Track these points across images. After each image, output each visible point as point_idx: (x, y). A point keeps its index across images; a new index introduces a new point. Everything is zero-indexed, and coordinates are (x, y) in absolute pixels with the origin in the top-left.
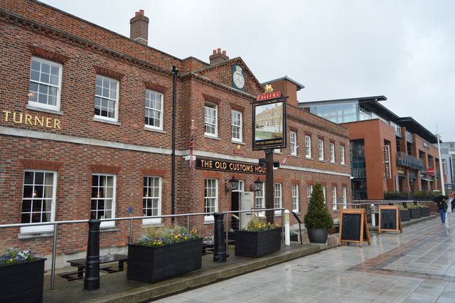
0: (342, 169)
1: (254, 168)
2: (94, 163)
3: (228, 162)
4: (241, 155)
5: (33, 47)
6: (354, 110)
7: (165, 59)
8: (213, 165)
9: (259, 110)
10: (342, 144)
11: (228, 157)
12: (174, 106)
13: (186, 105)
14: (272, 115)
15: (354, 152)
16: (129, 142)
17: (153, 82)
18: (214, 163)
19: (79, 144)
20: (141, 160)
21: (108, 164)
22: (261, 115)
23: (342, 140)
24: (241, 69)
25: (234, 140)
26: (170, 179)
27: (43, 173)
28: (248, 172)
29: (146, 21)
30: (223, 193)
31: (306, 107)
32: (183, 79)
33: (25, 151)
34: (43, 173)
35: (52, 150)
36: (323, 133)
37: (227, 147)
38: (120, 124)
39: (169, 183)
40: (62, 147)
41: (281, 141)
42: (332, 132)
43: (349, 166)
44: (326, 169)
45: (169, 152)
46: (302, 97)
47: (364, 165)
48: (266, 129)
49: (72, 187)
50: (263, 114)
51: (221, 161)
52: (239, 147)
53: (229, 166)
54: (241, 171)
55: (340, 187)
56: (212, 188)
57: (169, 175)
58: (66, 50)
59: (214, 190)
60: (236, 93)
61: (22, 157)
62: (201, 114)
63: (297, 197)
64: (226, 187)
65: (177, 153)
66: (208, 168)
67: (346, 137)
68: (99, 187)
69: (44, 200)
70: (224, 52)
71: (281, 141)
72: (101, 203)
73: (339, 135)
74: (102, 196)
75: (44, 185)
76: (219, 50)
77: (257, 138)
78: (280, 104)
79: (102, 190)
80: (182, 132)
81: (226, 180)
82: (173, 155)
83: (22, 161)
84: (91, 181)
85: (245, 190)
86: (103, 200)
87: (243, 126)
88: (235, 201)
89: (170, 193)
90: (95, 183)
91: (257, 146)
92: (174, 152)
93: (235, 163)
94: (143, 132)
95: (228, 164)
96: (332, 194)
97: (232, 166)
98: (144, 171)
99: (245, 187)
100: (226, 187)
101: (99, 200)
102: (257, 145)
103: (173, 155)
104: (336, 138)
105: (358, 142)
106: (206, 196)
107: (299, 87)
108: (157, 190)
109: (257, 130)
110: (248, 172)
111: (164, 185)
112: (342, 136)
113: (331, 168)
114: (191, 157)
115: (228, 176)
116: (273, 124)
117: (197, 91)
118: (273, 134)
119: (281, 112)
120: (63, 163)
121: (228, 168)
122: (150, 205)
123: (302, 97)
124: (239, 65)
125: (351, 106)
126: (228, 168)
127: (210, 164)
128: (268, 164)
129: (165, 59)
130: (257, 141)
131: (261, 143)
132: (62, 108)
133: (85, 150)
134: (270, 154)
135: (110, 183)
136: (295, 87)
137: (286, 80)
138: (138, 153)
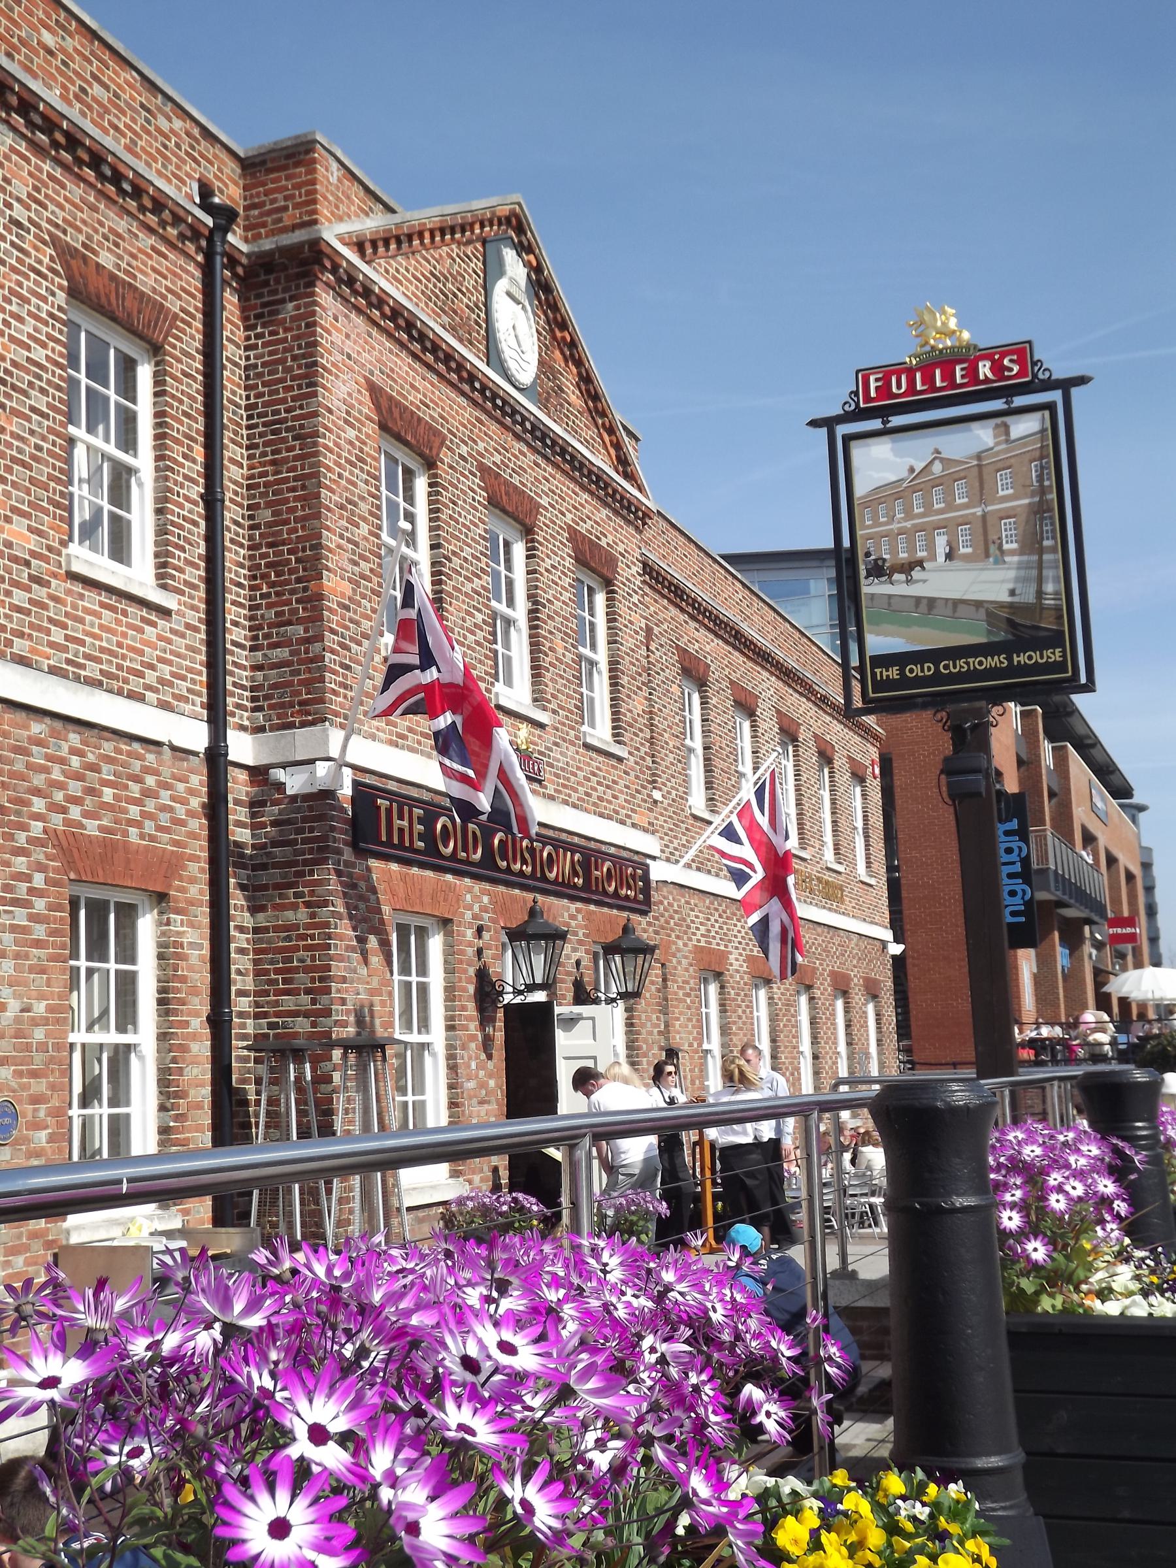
7: (163, 123)
8: (429, 836)
14: (982, 490)
17: (106, 259)
18: (429, 820)
20: (56, 775)
26: (203, 914)
27: (107, 902)
34: (107, 902)
39: (195, 938)
48: (942, 581)
50: (919, 483)
56: (414, 979)
62: (364, 508)
65: (242, 747)
77: (879, 642)
81: (480, 931)
82: (216, 757)
87: (533, 615)
89: (201, 1005)
94: (58, 586)
98: (69, 848)
109: (870, 588)
111: (167, 955)
116: (988, 548)
118: (990, 611)
129: (163, 123)
130: (883, 661)
138: (38, 728)
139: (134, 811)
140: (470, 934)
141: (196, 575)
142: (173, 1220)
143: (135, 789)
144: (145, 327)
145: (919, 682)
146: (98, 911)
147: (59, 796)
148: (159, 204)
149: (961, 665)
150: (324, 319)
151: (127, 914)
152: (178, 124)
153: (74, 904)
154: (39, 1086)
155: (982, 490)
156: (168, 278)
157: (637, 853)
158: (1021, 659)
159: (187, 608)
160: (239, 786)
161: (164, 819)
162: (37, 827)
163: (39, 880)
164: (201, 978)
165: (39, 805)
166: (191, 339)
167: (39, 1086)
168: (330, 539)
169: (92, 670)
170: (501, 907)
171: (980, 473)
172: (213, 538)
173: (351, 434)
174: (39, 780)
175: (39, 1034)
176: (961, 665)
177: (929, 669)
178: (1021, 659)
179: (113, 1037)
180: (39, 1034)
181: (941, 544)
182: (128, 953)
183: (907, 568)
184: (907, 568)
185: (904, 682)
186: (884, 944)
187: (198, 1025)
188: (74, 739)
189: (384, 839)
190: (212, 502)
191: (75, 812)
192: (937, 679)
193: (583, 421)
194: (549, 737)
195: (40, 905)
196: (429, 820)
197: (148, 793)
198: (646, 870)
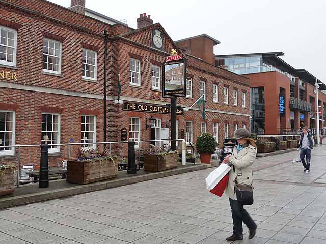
2: (43, 105)
6: (259, 63)
8: (137, 108)
12: (105, 62)
14: (177, 72)
18: (137, 106)
19: (31, 91)
20: (80, 103)
21: (54, 106)
26: (103, 118)
34: (89, 117)
35: (11, 96)
36: (227, 83)
39: (102, 121)
45: (103, 97)
46: (218, 51)
48: (172, 82)
58: (16, 17)
60: (155, 52)
70: (149, 16)
73: (241, 84)
76: (145, 14)
77: (166, 89)
78: (182, 64)
82: (105, 99)
84: (41, 119)
88: (153, 134)
92: (105, 97)
93: (154, 105)
95: (148, 107)
97: (151, 108)
101: (6, 132)
103: (105, 99)
104: (238, 86)
107: (216, 43)
111: (98, 123)
113: (234, 109)
116: (177, 79)
117: (124, 50)
118: (178, 86)
123: (218, 51)
130: (166, 91)
133: (36, 95)
134: (174, 101)
137: (205, 37)
138: (77, 98)
139: (92, 106)
142: (15, 177)
146: (134, 119)
147: (80, 105)
149: (174, 92)
150: (248, 211)
151: (137, 119)
153: (130, 119)
155: (177, 72)
157: (275, 154)
161: (97, 107)
162: (77, 109)
165: (77, 107)
166: (103, 50)
176: (174, 92)
187: (102, 130)
188: (83, 99)
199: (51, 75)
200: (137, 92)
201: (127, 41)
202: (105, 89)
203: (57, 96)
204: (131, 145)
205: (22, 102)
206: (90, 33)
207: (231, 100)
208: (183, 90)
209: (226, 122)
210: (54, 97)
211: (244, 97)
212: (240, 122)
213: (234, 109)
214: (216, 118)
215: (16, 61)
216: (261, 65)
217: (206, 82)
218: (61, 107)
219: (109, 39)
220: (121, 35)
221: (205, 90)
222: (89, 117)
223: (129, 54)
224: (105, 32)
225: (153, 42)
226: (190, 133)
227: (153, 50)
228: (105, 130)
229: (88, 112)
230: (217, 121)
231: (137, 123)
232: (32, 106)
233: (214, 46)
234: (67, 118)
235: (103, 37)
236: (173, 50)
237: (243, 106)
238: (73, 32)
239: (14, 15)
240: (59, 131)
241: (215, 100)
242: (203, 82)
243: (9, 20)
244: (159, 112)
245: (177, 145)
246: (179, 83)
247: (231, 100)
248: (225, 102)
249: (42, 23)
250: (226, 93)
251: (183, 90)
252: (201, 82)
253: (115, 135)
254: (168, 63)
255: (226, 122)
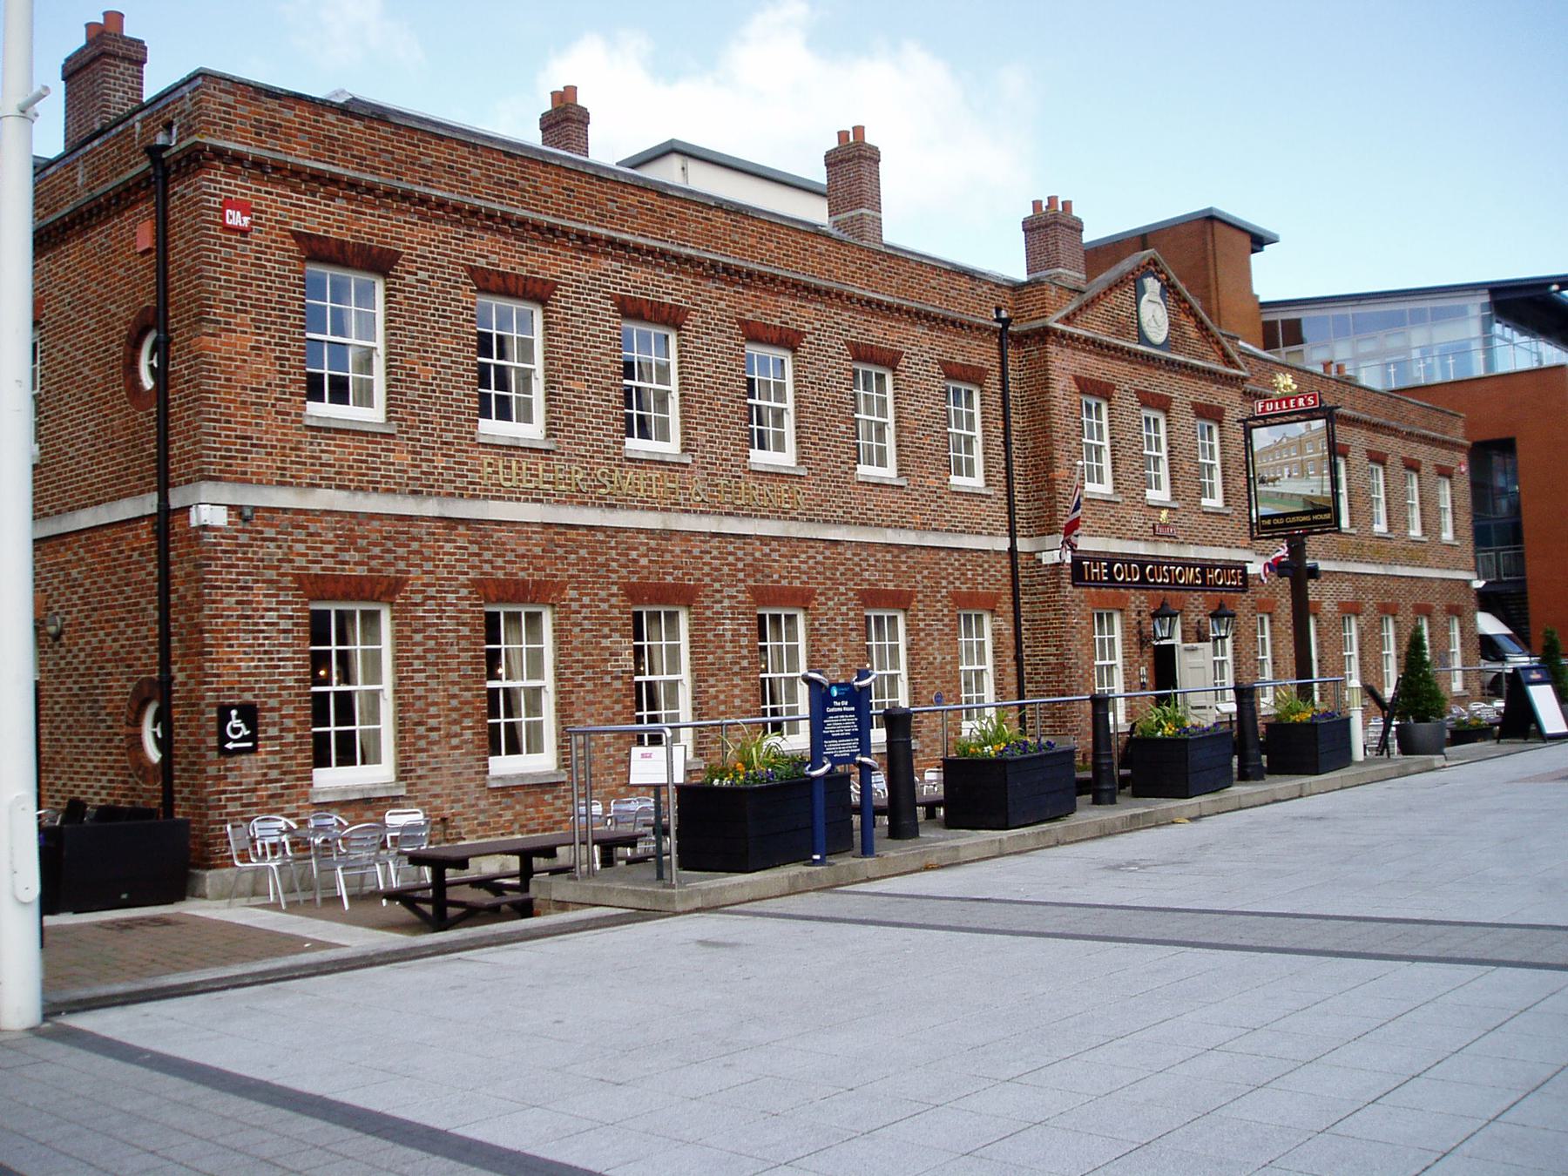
0: (1446, 556)
1: (1203, 573)
2: (865, 586)
3: (1142, 562)
4: (1172, 539)
5: (747, 322)
6: (1474, 328)
8: (1110, 574)
9: (1263, 437)
10: (1445, 472)
11: (1141, 549)
12: (1006, 418)
13: (1040, 412)
14: (1301, 451)
15: (1481, 492)
16: (924, 527)
17: (959, 359)
18: (1110, 567)
19: (836, 542)
21: (891, 586)
22: (1269, 451)
23: (1444, 457)
24: (1157, 285)
25: (1152, 495)
26: (1010, 616)
28: (1190, 587)
29: (873, 156)
30: (1135, 648)
31: (1283, 328)
32: (1021, 340)
33: (754, 569)
34: (498, 614)
36: (1384, 443)
37: (1136, 519)
38: (902, 482)
39: (1007, 628)
40: (811, 552)
41: (1328, 516)
42: (1409, 436)
43: (1469, 547)
44: (1395, 561)
45: (1003, 544)
46: (1271, 278)
47: (1513, 533)
48: (1287, 486)
49: (833, 646)
51: (1127, 559)
52: (1164, 513)
53: (1144, 572)
54: (1174, 585)
55: (1440, 618)
57: (1006, 606)
59: (894, 650)
60: (1148, 360)
61: (751, 582)
63: (1268, 656)
64: (1140, 632)
65: (1023, 545)
66: (1097, 583)
67: (1453, 446)
68: (334, 648)
69: (649, 683)
70: (1067, 205)
71: (1328, 516)
72: (345, 700)
73: (1433, 442)
74: (346, 677)
75: (503, 646)
76: (1053, 200)
78: (1319, 424)
79: (344, 658)
80: (1034, 482)
81: (1139, 613)
82: (1013, 551)
83: (753, 590)
84: (303, 632)
85: (1184, 640)
86: (349, 694)
88: (1164, 667)
89: (1010, 653)
90: (320, 636)
91: (1265, 528)
92: (1013, 542)
93: (1158, 562)
95: (1143, 566)
96: (1342, 644)
99: (1183, 631)
100: (1140, 632)
101: (336, 693)
102: (1265, 527)
103: (1013, 551)
104: (1421, 452)
105: (1489, 454)
106: (493, 676)
107: (1258, 241)
108: (373, 660)
110: (1190, 587)
111: (997, 634)
112: (1443, 444)
113: (1415, 552)
114: (1053, 554)
115: (1138, 600)
116: (1303, 474)
117: (1064, 365)
118: (1308, 500)
119: (1323, 446)
120: (813, 591)
121: (1143, 579)
122: (346, 715)
123: (1271, 278)
124: (1152, 274)
125: (1461, 313)
126: (1143, 579)
127: (1099, 570)
128: (1296, 572)
130: (1264, 517)
131: (1276, 521)
132: (802, 459)
134: (1297, 550)
135: (372, 633)
136: (1246, 241)
137: (1210, 220)
138: (942, 554)
140: (1134, 615)
141: (1000, 477)
143: (980, 571)
144: (975, 376)
145: (1278, 526)
148: (979, 327)
149: (1294, 520)
152: (985, 288)
154: (950, 686)
155: (1301, 451)
156: (982, 354)
158: (1316, 517)
159: (998, 492)
160: (1022, 561)
163: (946, 611)
164: (1011, 642)
165: (944, 583)
167: (950, 686)
168: (1057, 454)
169: (961, 527)
170: (1151, 601)
171: (1300, 444)
172: (1008, 460)
173: (1066, 403)
174: (944, 574)
175: (949, 667)
176: (1294, 520)
177: (1281, 521)
178: (1316, 517)
179: (976, 667)
180: (949, 667)
181: (1286, 470)
182: (980, 634)
183: (1273, 480)
184: (1273, 480)
185: (1272, 526)
186: (1467, 583)
187: (1010, 661)
188: (956, 555)
189: (855, 799)
190: (1007, 444)
191: (957, 583)
192: (1285, 525)
193: (1201, 347)
194: (1179, 514)
195: (946, 620)
196: (1110, 567)
197: (985, 571)
198: (1245, 569)
199: (877, 485)
200: (1107, 515)
201: (1071, 336)
202: (1011, 512)
203: (896, 552)
204: (1101, 704)
205: (820, 578)
206: (970, 327)
207: (1396, 517)
208: (1327, 510)
209: (1385, 612)
210: (889, 557)
211: (1445, 492)
212: (1438, 606)
213: (1415, 552)
214: (1348, 593)
215: (794, 451)
216: (1488, 341)
217: (1166, 412)
218: (905, 587)
219: (1011, 335)
220: (1054, 322)
221: (1106, 443)
222: (498, 614)
223: (1077, 379)
224: (998, 310)
225: (1139, 327)
226: (979, 674)
227: (1142, 354)
228: (1018, 659)
229: (515, 591)
230: (1351, 609)
231: (792, 635)
232: (842, 589)
233: (1254, 257)
234: (922, 625)
235: (995, 332)
236: (1280, 378)
237: (1412, 533)
238: (918, 331)
239: (785, 302)
240: (1355, 652)
241: (1160, 495)
242: (1152, 414)
243: (777, 322)
244: (1174, 585)
245: (1317, 698)
246: (1314, 486)
247: (1396, 517)
248: (1205, 502)
249: (846, 315)
250: (1212, 450)
251: (1327, 510)
252: (1145, 413)
253: (1053, 677)
254: (1266, 420)
255: (1387, 610)
